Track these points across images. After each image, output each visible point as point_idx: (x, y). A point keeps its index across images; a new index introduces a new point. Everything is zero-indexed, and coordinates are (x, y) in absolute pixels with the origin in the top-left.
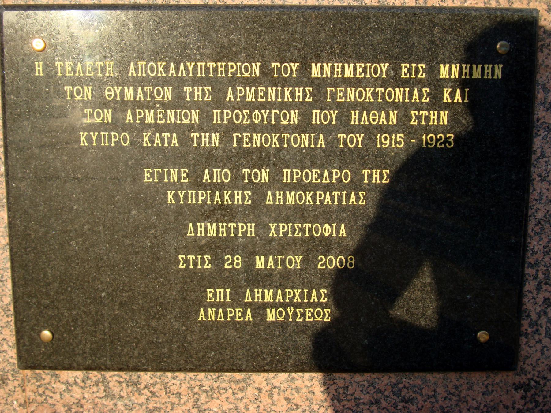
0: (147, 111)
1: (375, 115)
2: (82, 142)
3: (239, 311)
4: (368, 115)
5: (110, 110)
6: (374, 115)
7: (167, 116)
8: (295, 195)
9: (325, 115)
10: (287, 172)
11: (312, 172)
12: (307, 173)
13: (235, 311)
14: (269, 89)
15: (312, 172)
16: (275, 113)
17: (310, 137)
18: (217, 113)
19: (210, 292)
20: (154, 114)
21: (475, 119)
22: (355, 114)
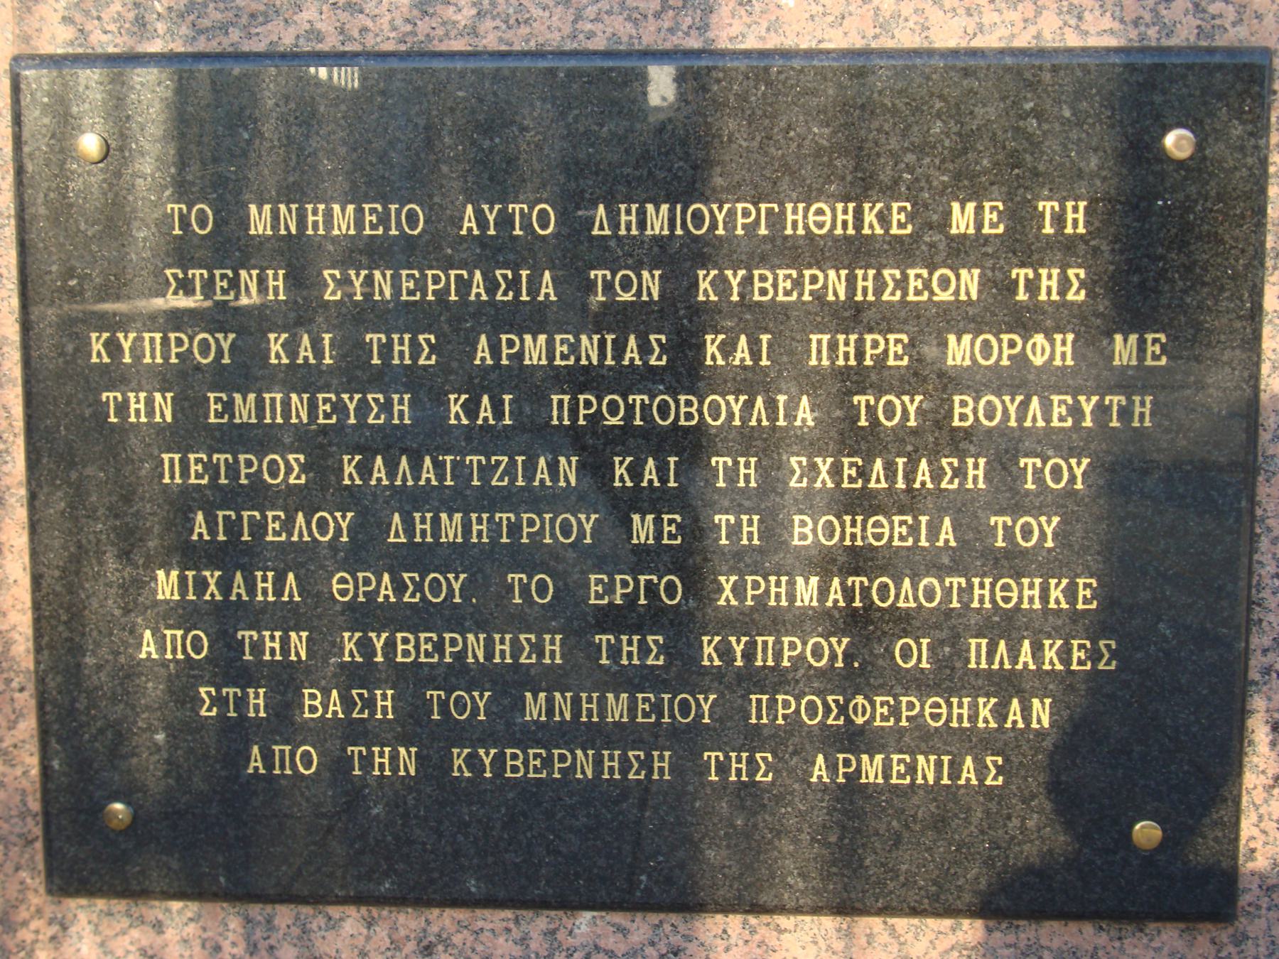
0: (865, 757)
1: (938, 706)
2: (273, 355)
3: (897, 341)
4: (915, 586)
5: (1048, 701)
6: (689, 403)
7: (233, 409)
8: (973, 344)
9: (684, 703)
10: (819, 342)
11: (1000, 341)
12: (986, 342)
13: (887, 341)
14: (584, 338)
15: (1000, 341)
16: (649, 582)
17: (602, 343)
18: (561, 402)
19: (1155, 341)
20: (976, 214)
21: (1244, 701)
22: (628, 212)
